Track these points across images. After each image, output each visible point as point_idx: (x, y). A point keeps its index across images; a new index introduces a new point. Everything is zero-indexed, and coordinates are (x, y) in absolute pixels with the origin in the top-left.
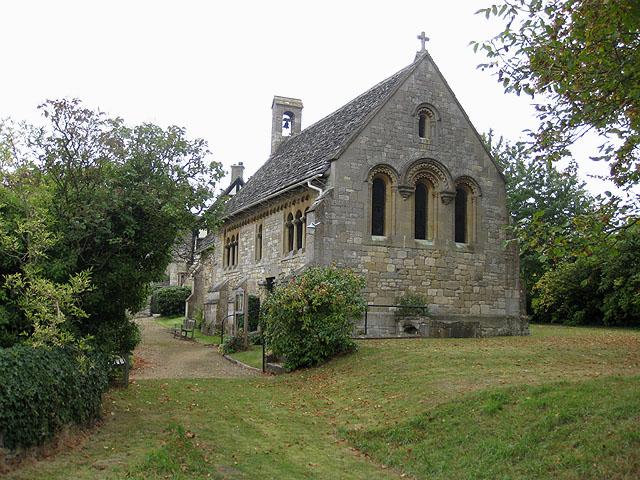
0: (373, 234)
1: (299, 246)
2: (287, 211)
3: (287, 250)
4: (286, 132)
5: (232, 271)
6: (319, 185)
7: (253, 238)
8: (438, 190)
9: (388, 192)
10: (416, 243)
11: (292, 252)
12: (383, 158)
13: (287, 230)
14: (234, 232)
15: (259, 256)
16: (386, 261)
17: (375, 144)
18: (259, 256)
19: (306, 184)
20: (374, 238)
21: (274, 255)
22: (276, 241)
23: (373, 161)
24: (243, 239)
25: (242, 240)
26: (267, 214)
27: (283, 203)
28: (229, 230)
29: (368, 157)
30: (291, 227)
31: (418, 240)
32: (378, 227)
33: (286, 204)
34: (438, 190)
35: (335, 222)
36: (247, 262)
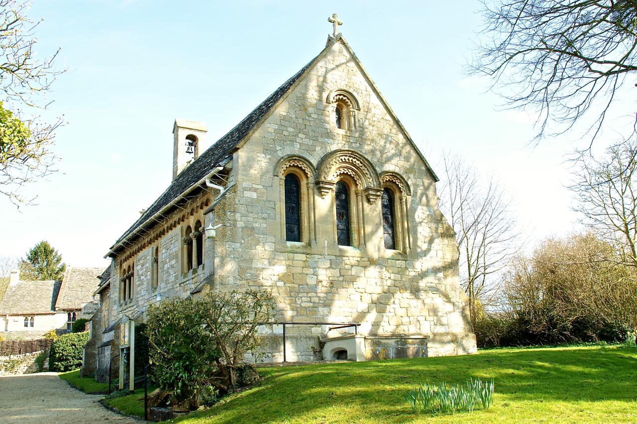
0: (289, 239)
1: (200, 262)
2: (184, 225)
3: (186, 270)
4: (232, 421)
5: (128, 305)
6: (220, 183)
7: (148, 265)
8: (360, 188)
9: (304, 189)
10: (341, 250)
11: (192, 271)
12: (296, 150)
13: (185, 246)
14: (130, 262)
15: (154, 287)
16: (306, 271)
17: (285, 133)
18: (154, 287)
19: (204, 184)
20: (289, 244)
21: (172, 279)
22: (173, 262)
23: (284, 151)
24: (139, 267)
25: (138, 268)
26: (163, 233)
27: (180, 215)
28: (125, 260)
29: (278, 148)
30: (189, 243)
31: (341, 247)
32: (294, 230)
33: (184, 216)
34: (360, 188)
35: (240, 224)
36: (143, 293)
